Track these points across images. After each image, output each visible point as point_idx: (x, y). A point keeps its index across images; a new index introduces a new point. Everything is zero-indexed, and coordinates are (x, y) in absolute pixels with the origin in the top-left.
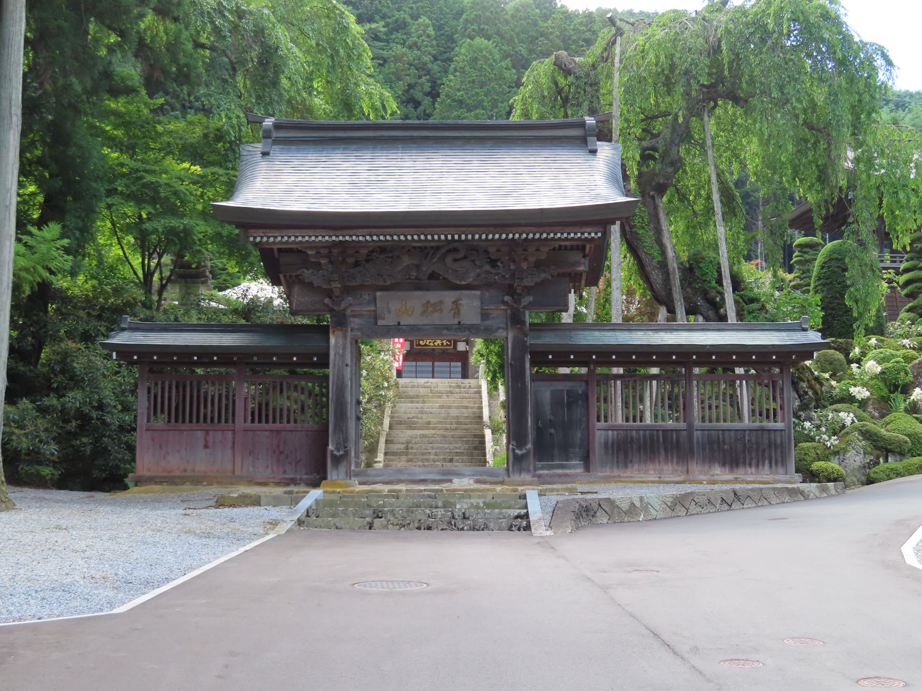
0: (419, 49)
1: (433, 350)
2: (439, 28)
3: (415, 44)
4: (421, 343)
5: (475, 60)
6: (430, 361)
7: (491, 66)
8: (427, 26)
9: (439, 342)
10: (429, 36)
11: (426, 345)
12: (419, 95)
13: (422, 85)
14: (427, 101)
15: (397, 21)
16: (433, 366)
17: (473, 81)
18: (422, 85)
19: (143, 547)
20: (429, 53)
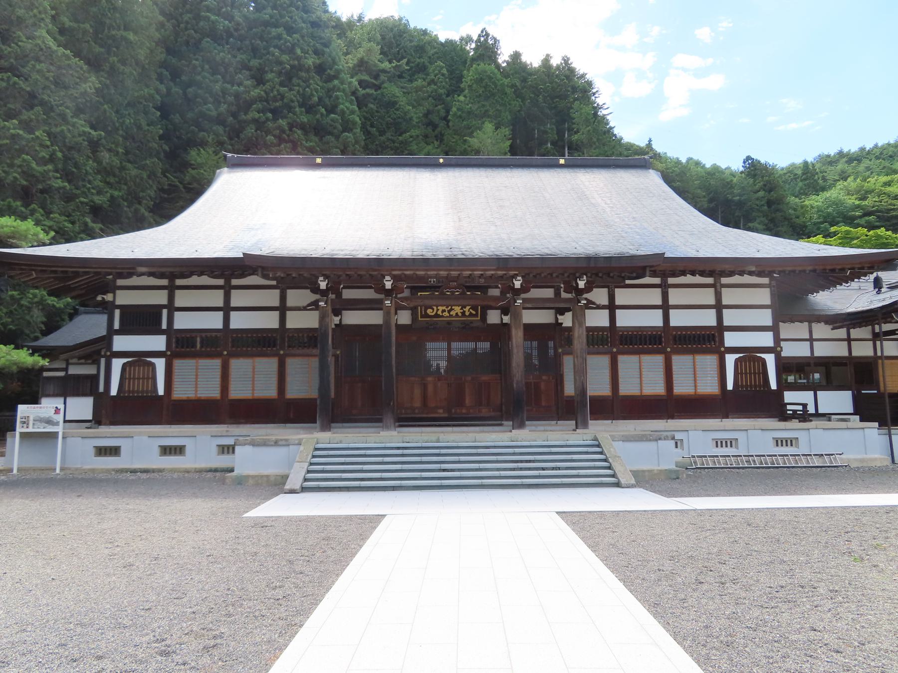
0: (435, 84)
1: (449, 323)
2: (451, 72)
3: (433, 81)
4: (429, 311)
5: (481, 80)
6: (443, 340)
7: (494, 83)
8: (442, 68)
9: (457, 309)
10: (443, 75)
11: (437, 316)
12: (435, 118)
13: (438, 111)
14: (442, 124)
15: (418, 65)
16: (196, 393)
17: (480, 95)
18: (438, 111)
19: (75, 664)
20: (444, 87)
